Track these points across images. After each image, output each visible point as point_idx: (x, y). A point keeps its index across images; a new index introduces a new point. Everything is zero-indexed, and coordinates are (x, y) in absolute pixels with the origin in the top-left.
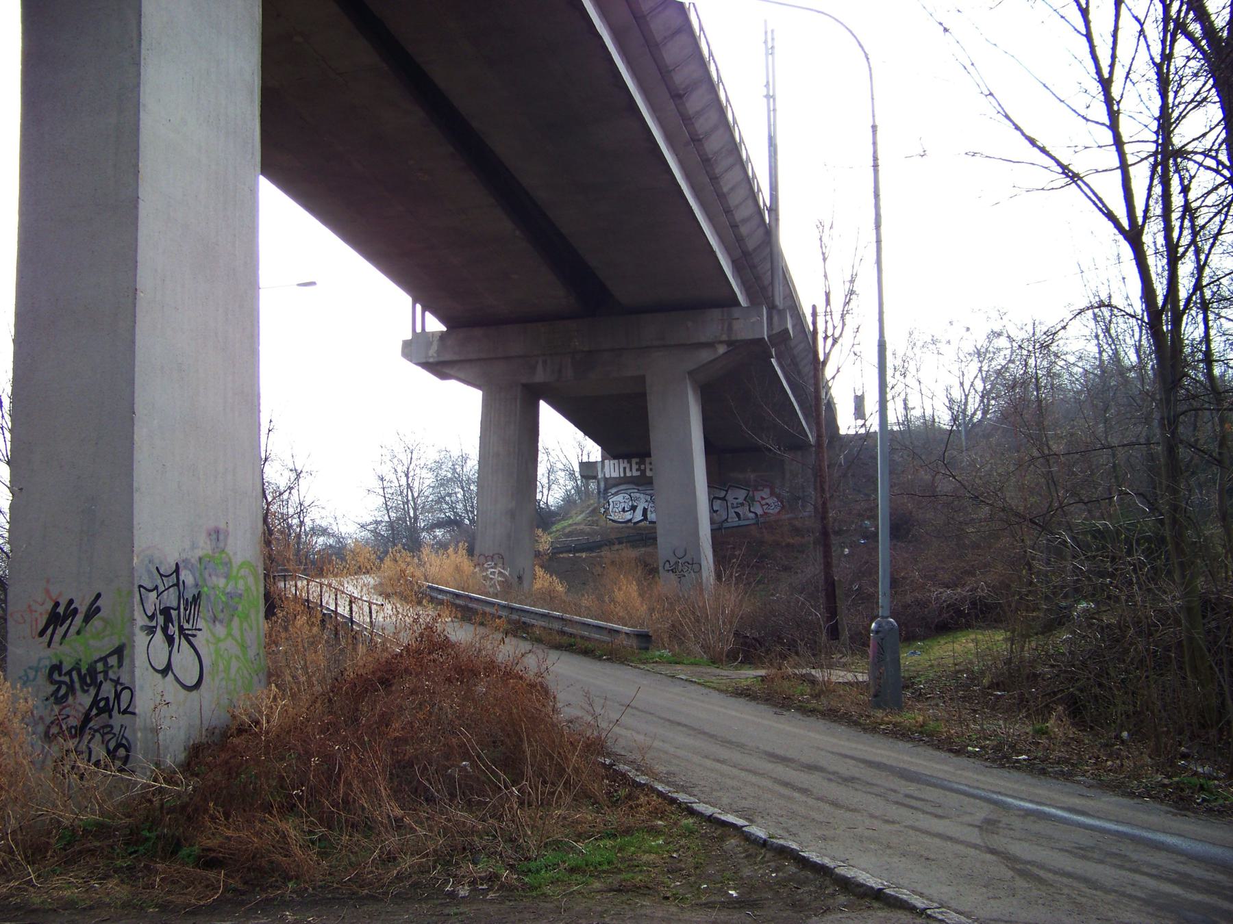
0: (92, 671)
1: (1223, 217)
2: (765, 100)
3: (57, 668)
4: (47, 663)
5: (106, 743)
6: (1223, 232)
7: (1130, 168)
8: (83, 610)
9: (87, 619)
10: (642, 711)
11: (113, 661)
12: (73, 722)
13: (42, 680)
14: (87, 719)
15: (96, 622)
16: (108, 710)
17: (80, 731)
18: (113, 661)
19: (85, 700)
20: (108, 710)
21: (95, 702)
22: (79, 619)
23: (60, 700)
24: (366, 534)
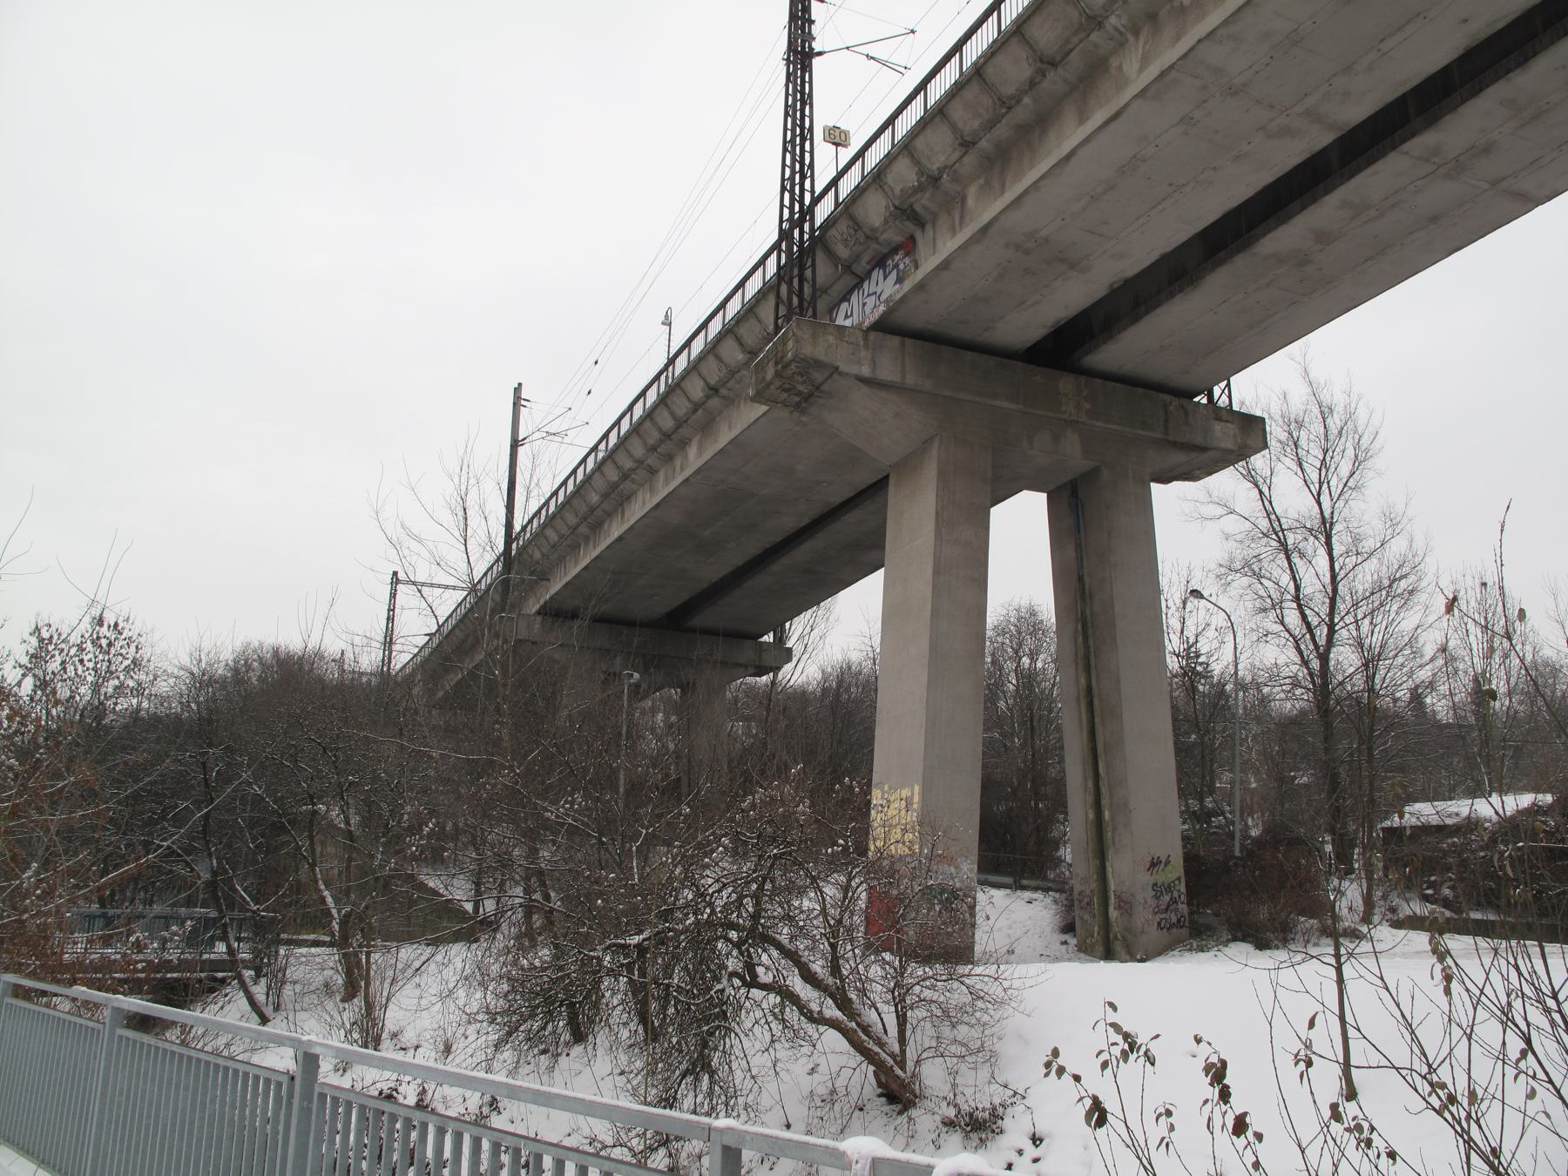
0: (1169, 886)
1: (1314, 621)
2: (813, 18)
3: (1155, 885)
4: (1151, 883)
5: (1176, 915)
6: (1339, 578)
7: (1232, 467)
8: (1164, 861)
9: (1165, 865)
10: (1257, 486)
11: (1177, 882)
12: (1163, 907)
13: (1150, 888)
14: (1168, 906)
15: (1169, 867)
16: (1176, 902)
17: (1166, 910)
18: (1177, 882)
19: (1167, 898)
20: (1176, 902)
21: (1171, 899)
22: (1162, 865)
23: (1158, 898)
24: (1055, 834)
